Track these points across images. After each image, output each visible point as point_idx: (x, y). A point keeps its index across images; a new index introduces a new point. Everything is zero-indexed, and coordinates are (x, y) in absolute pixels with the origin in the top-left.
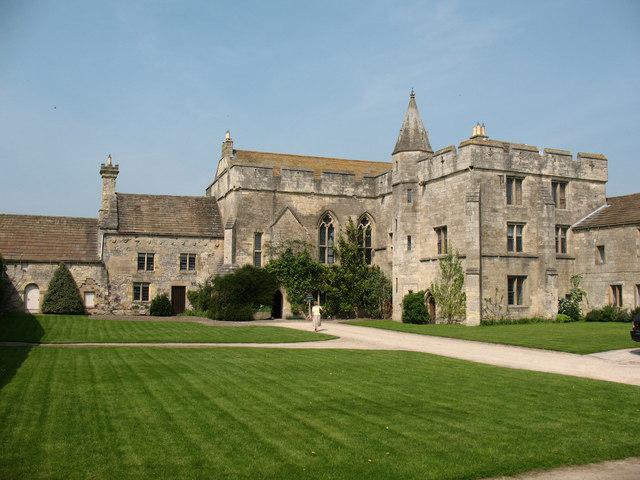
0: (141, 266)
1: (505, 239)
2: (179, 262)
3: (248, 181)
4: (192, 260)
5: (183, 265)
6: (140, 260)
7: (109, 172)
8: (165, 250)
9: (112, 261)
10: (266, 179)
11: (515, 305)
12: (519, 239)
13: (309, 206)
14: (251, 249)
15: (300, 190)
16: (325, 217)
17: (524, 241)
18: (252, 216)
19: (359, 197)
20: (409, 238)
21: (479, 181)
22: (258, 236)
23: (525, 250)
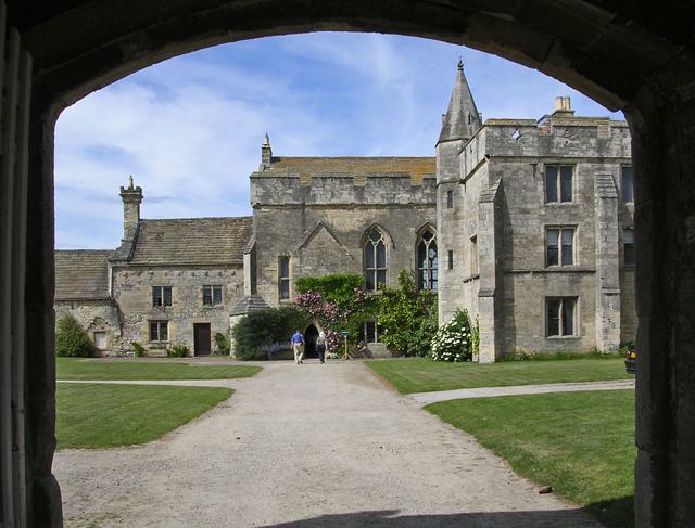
0: (157, 302)
1: (542, 249)
2: (201, 296)
3: (267, 195)
4: (218, 292)
5: (207, 299)
6: (206, 292)
7: (132, 197)
8: (182, 283)
9: (123, 298)
10: (290, 191)
11: (560, 336)
12: (567, 249)
13: (351, 221)
14: (276, 278)
15: (335, 201)
16: (371, 232)
17: (576, 249)
18: (275, 237)
19: (419, 205)
20: (451, 253)
21: (500, 173)
22: (284, 261)
23: (577, 262)
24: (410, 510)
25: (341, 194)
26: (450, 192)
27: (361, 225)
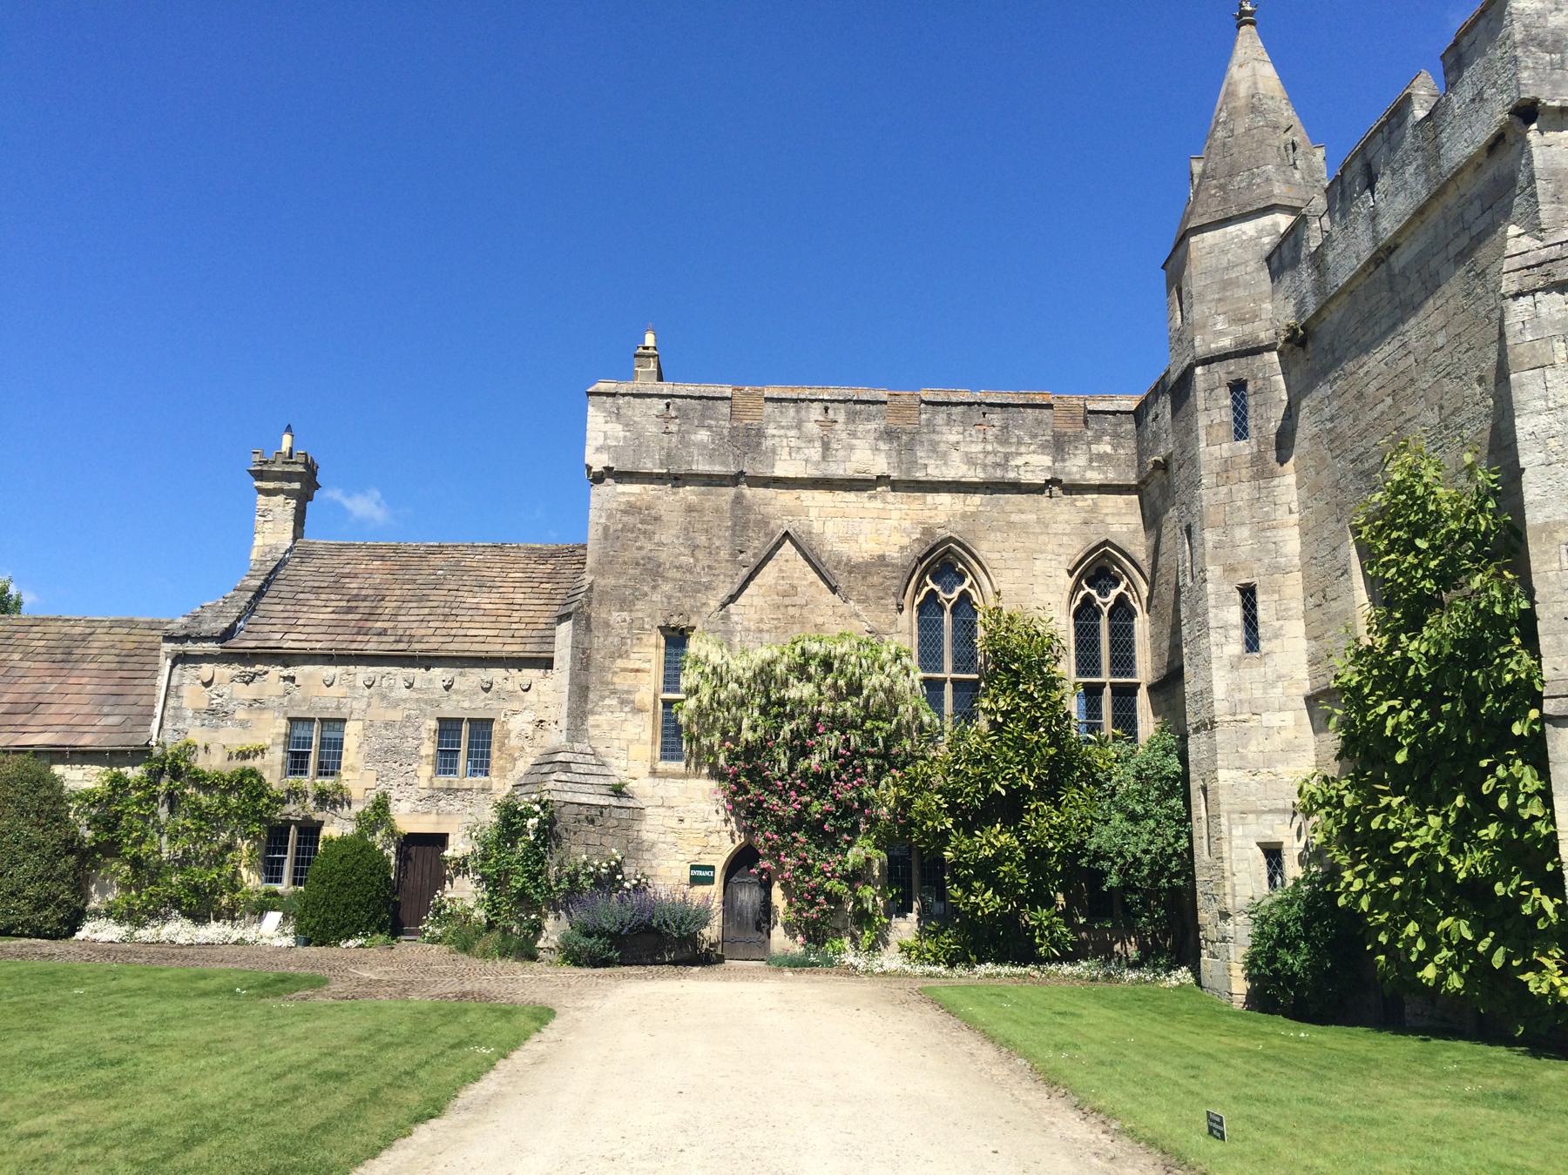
2: (428, 749)
5: (445, 760)
13: (882, 529)
15: (837, 470)
18: (653, 570)
20: (1248, 594)
22: (676, 638)
24: (1463, 1045)
25: (852, 448)
26: (1238, 387)
27: (906, 541)
